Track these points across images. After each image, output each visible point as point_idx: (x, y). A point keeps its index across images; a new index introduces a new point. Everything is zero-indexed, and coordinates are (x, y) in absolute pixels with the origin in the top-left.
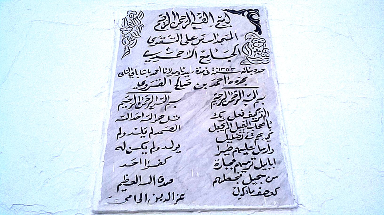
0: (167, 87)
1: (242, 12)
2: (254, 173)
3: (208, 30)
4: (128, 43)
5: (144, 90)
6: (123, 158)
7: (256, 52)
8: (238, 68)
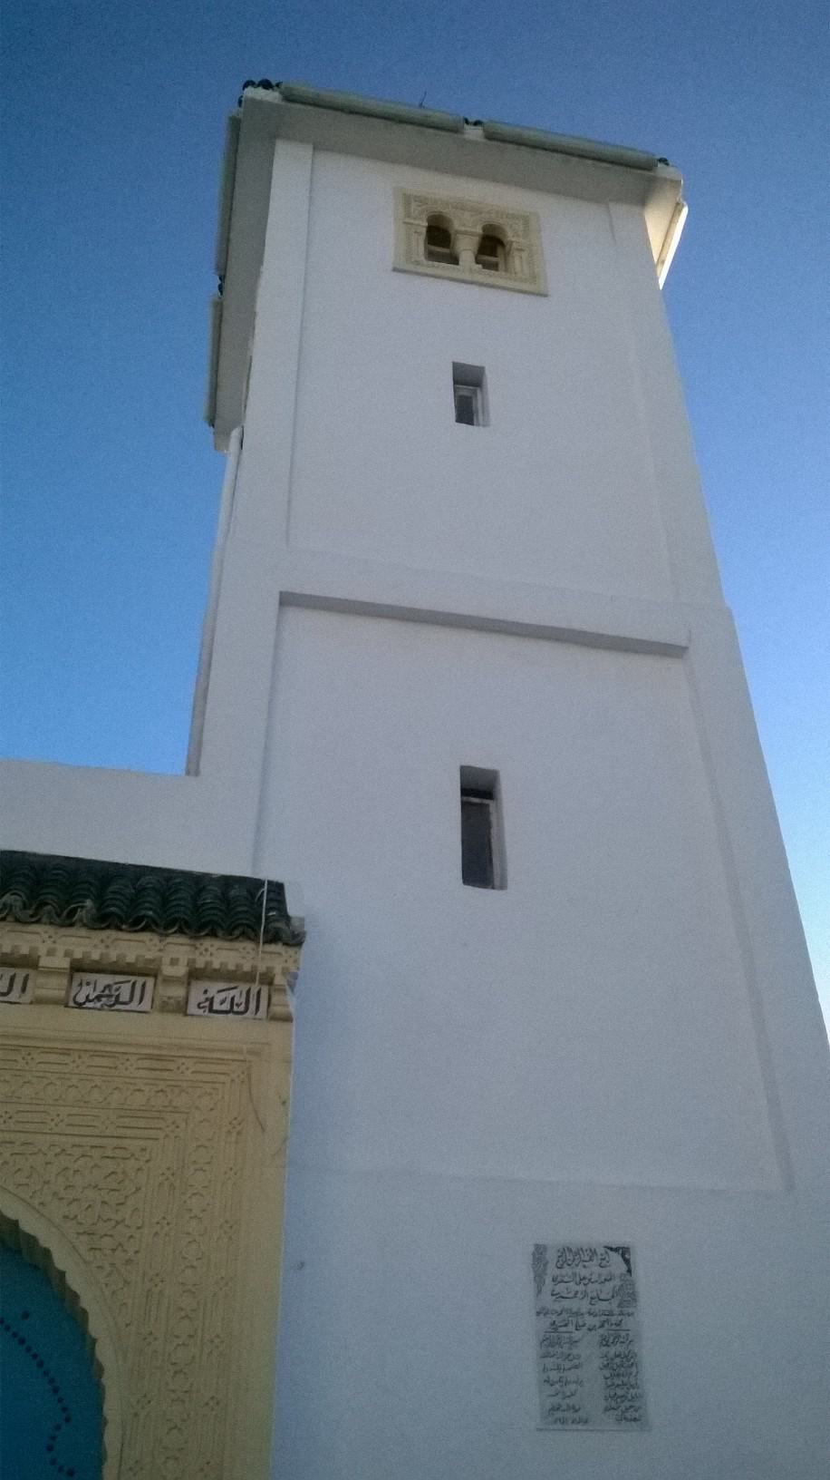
0: (571, 1328)
1: (616, 1250)
2: (628, 1404)
3: (593, 1269)
4: (539, 1278)
5: (556, 1330)
6: (552, 1390)
7: (627, 1296)
8: (617, 1311)
